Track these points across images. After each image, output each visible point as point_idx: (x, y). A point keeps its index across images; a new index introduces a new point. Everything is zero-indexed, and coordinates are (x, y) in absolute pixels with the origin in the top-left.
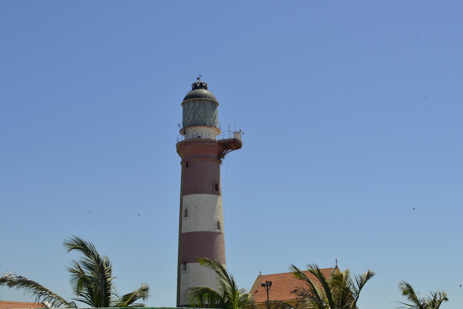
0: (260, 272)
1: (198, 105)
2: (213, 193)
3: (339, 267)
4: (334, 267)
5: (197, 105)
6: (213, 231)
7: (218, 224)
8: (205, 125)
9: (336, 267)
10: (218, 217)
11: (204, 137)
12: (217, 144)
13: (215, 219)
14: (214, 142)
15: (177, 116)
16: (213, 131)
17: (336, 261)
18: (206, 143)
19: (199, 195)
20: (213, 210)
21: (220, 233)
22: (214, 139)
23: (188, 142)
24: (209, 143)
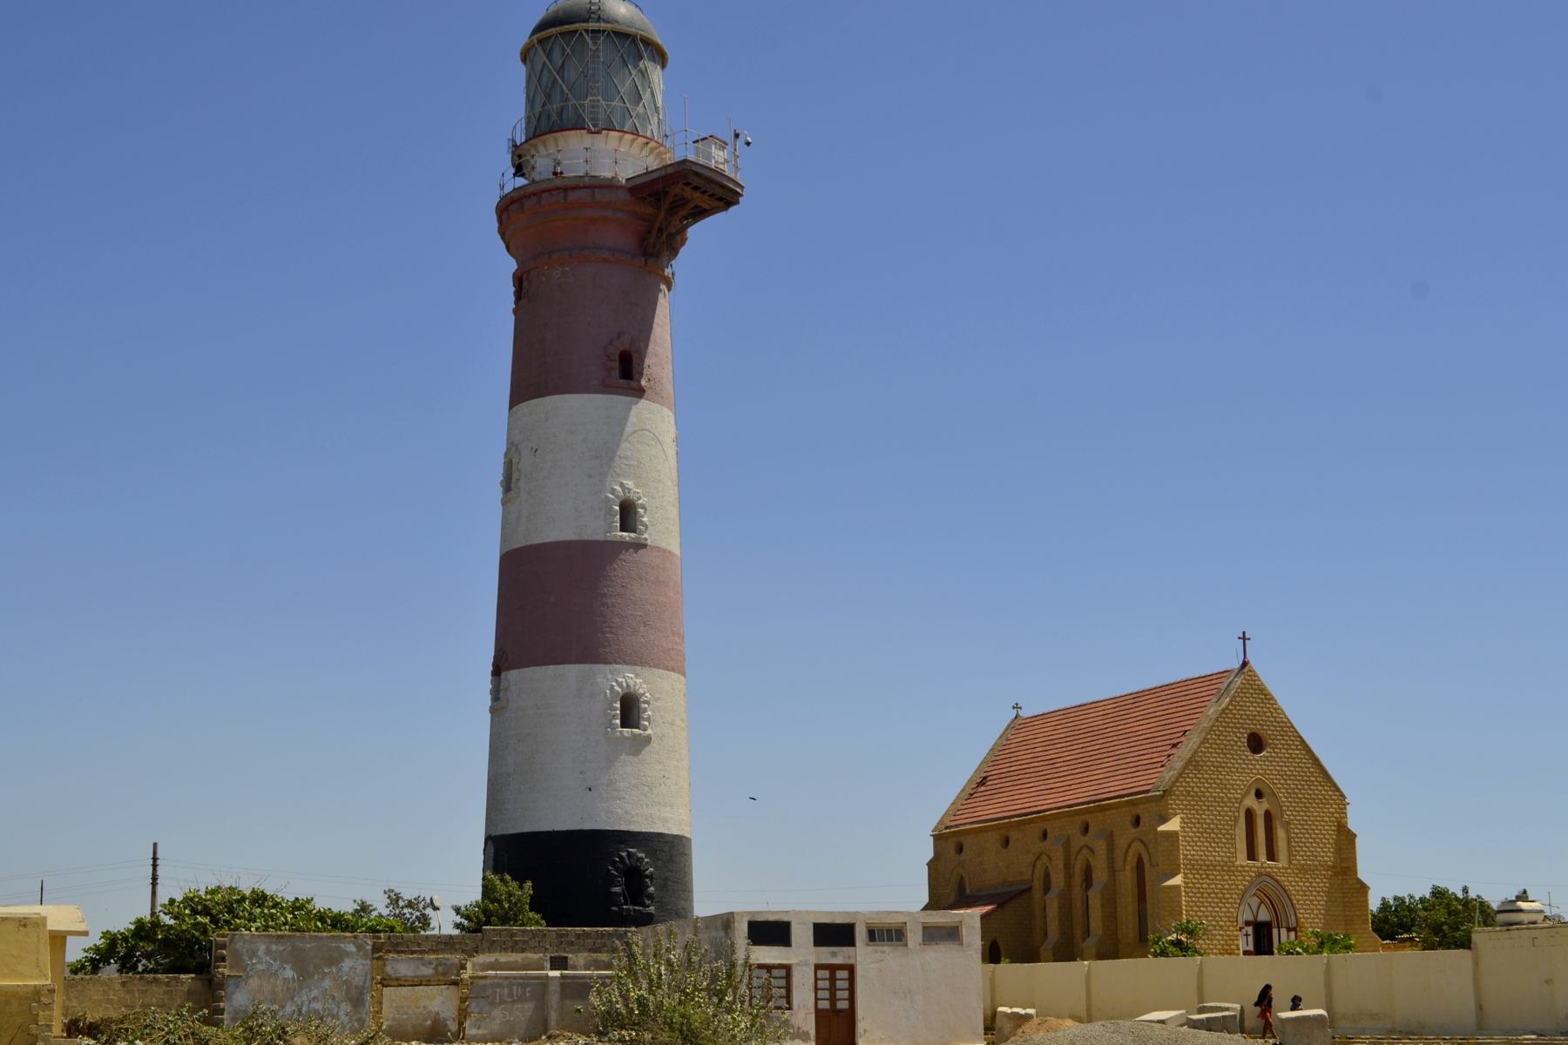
0: (1016, 707)
1: (575, 60)
2: (606, 388)
3: (1254, 663)
4: (1237, 665)
5: (557, 54)
6: (599, 537)
7: (628, 514)
8: (578, 125)
9: (1245, 664)
10: (629, 484)
11: (574, 167)
12: (623, 196)
13: (613, 491)
14: (610, 185)
15: (508, 109)
16: (635, 150)
17: (1244, 638)
18: (573, 196)
19: (548, 398)
20: (605, 454)
21: (640, 546)
22: (609, 175)
23: (513, 202)
24: (583, 195)
